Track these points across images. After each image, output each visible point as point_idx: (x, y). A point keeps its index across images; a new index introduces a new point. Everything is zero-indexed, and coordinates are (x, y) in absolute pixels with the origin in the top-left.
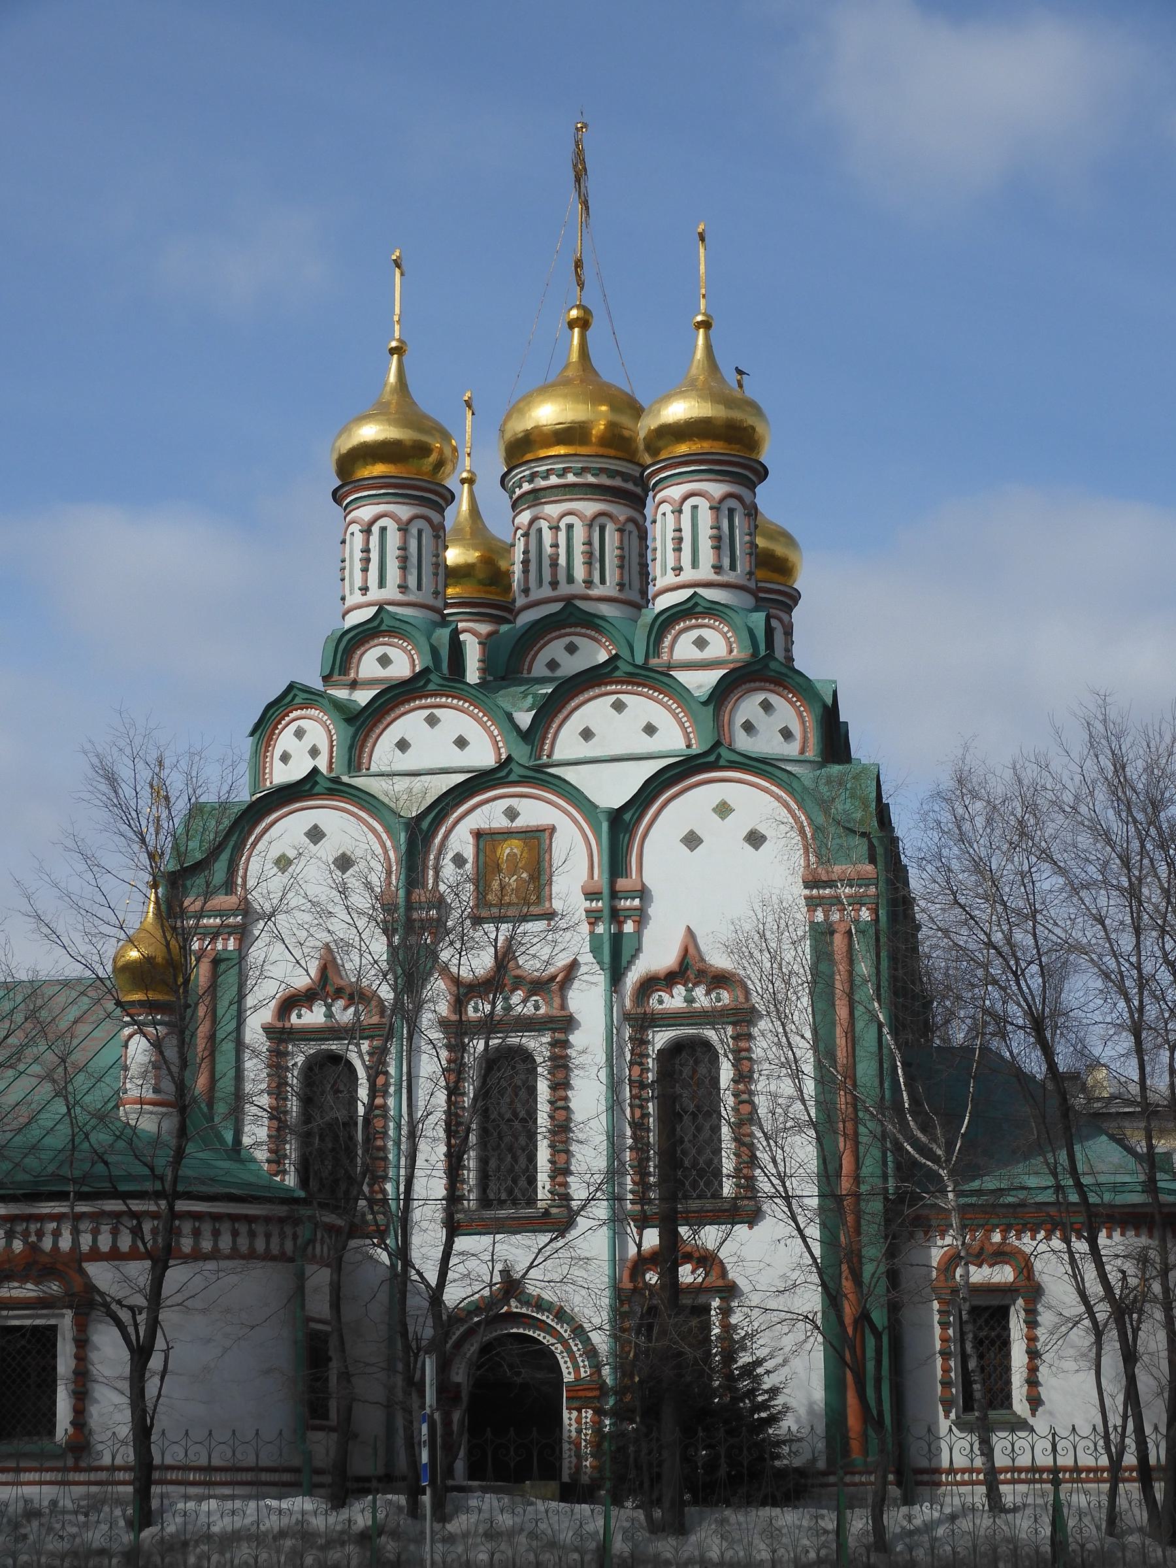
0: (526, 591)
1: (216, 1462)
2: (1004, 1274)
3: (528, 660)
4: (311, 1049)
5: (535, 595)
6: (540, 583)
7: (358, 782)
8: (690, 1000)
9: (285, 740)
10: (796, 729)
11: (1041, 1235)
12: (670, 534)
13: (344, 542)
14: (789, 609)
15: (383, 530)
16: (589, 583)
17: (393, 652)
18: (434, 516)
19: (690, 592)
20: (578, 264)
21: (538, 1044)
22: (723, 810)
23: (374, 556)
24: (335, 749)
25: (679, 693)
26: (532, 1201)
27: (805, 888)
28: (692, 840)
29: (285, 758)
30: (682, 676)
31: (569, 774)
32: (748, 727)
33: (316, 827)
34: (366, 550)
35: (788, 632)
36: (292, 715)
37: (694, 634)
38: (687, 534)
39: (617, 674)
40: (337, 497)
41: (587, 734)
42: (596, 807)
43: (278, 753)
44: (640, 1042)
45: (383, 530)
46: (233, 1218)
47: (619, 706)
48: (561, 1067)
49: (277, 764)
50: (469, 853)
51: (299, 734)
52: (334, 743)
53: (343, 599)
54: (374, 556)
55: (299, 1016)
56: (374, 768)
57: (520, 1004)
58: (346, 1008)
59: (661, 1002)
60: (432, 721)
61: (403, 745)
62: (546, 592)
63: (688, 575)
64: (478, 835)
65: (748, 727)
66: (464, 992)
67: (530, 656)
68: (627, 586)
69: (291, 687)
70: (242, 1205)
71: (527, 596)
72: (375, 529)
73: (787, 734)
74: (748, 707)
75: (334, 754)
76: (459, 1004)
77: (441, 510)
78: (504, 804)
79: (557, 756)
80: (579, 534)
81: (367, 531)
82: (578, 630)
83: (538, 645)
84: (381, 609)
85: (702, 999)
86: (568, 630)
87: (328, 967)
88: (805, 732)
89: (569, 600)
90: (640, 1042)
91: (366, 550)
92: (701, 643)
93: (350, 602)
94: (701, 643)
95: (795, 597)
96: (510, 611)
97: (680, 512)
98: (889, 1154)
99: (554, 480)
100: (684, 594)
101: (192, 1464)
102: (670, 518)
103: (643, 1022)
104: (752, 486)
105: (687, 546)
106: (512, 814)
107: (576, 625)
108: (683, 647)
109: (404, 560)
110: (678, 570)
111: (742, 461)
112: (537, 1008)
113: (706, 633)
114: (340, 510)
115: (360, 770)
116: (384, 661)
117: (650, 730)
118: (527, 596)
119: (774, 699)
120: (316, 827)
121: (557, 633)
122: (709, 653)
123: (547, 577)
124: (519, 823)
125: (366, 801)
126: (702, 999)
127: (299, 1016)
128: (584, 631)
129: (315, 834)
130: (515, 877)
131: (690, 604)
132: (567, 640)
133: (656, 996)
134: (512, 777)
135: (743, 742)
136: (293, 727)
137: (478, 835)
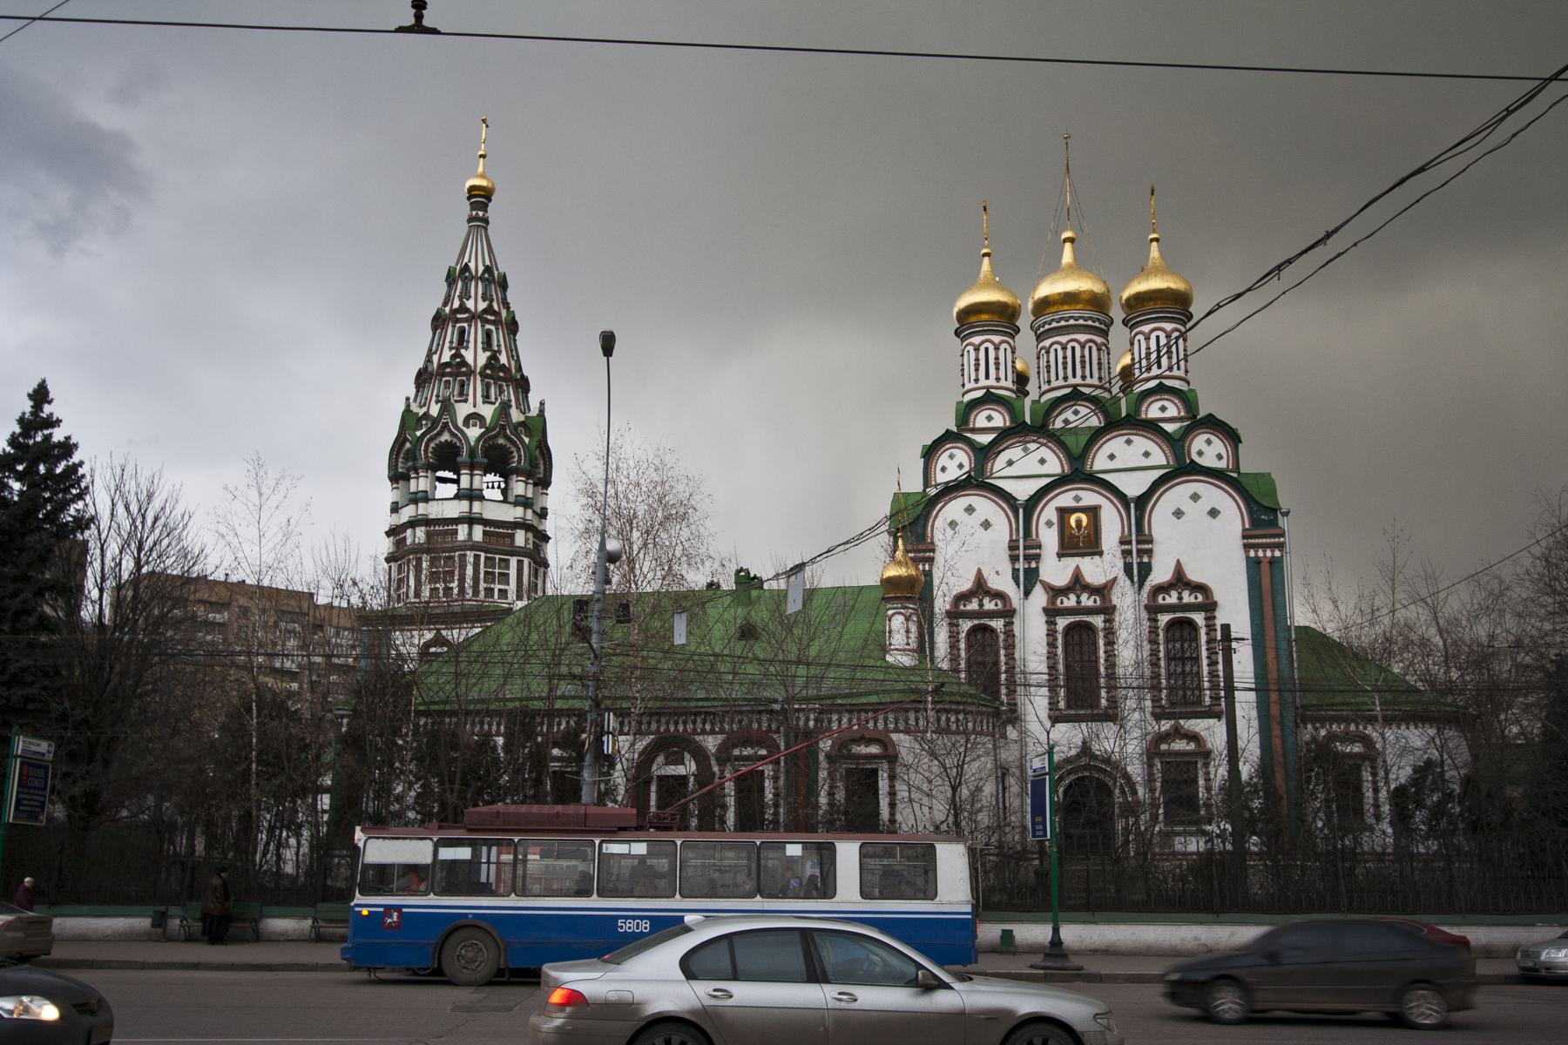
2: (1357, 748)
4: (1072, 619)
5: (1054, 384)
6: (1057, 379)
8: (1180, 598)
9: (943, 460)
10: (1224, 454)
11: (1403, 727)
12: (973, 362)
13: (962, 355)
15: (987, 349)
16: (1170, 368)
17: (994, 414)
21: (1098, 621)
23: (982, 363)
26: (1098, 705)
29: (943, 469)
34: (977, 359)
37: (1159, 404)
40: (957, 333)
41: (1112, 457)
44: (1153, 620)
47: (1129, 442)
48: (1110, 633)
53: (963, 385)
54: (982, 363)
55: (965, 606)
57: (1087, 601)
58: (1088, 598)
59: (1062, 603)
61: (1112, 457)
62: (1061, 382)
66: (1055, 592)
69: (947, 431)
73: (1220, 457)
76: (1052, 600)
78: (1074, 493)
80: (1163, 341)
81: (977, 349)
85: (1187, 598)
87: (980, 581)
88: (1228, 456)
89: (1075, 387)
90: (1153, 620)
91: (977, 359)
92: (989, 418)
93: (968, 386)
94: (989, 418)
97: (1149, 338)
102: (1143, 342)
103: (1153, 610)
104: (1013, 337)
106: (1077, 499)
108: (980, 420)
109: (997, 364)
110: (977, 380)
113: (1166, 403)
114: (959, 340)
117: (1147, 454)
119: (1213, 438)
123: (973, 377)
124: (1082, 504)
126: (1187, 598)
127: (965, 606)
129: (970, 510)
136: (948, 452)
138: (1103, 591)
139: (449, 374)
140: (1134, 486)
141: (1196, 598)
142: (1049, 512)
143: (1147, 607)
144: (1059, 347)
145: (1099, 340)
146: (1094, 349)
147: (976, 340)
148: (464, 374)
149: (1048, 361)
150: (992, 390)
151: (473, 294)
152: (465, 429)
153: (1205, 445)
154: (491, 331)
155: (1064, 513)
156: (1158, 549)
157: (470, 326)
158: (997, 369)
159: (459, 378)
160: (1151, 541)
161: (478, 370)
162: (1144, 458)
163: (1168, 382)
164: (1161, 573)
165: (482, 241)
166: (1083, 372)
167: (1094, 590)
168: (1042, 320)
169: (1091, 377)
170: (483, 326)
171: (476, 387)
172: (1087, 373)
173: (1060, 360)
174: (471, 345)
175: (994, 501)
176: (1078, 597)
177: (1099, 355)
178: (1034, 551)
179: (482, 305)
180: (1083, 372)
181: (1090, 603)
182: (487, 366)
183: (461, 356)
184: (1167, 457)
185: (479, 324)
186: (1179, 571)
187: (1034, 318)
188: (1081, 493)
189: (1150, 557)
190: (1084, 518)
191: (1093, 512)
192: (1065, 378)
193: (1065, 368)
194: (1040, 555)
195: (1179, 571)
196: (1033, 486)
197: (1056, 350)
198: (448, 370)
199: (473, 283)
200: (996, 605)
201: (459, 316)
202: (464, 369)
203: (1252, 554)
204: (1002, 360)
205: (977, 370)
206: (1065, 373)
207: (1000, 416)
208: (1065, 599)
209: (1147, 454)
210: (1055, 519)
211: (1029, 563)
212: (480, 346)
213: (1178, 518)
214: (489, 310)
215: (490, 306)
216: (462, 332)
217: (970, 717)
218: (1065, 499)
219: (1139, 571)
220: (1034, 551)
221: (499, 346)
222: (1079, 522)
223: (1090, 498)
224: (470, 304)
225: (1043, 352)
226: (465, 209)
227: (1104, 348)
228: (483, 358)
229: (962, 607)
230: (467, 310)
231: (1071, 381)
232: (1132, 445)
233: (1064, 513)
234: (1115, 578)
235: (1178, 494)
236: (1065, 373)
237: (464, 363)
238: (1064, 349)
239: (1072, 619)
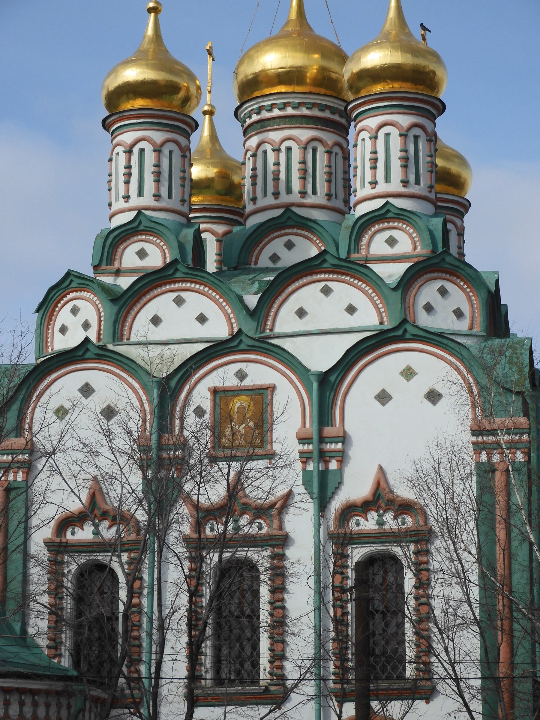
0: (254, 200)
3: (255, 254)
4: (83, 559)
5: (261, 203)
7: (121, 349)
8: (381, 523)
10: (466, 310)
12: (368, 156)
14: (462, 216)
15: (142, 151)
16: (303, 194)
23: (135, 171)
24: (102, 323)
27: (473, 435)
29: (63, 330)
30: (377, 268)
31: (287, 344)
32: (429, 308)
33: (87, 384)
34: (128, 167)
35: (461, 234)
36: (69, 296)
37: (386, 234)
38: (381, 155)
39: (326, 265)
41: (301, 313)
43: (57, 326)
46: (21, 691)
47: (326, 291)
49: (57, 334)
50: (207, 406)
51: (75, 311)
52: (102, 319)
53: (110, 205)
54: (135, 171)
55: (73, 533)
56: (133, 339)
58: (110, 527)
59: (358, 524)
60: (179, 302)
62: (270, 200)
63: (382, 188)
64: (215, 392)
65: (429, 308)
67: (257, 251)
68: (334, 196)
69: (69, 274)
71: (255, 204)
72: (136, 150)
73: (459, 314)
75: (102, 328)
76: (198, 526)
77: (187, 136)
78: (235, 367)
79: (278, 330)
82: (295, 230)
83: (263, 243)
84: (139, 213)
86: (287, 231)
89: (287, 207)
91: (128, 167)
95: (466, 206)
96: (241, 215)
97: (376, 138)
99: (276, 112)
102: (368, 143)
104: (433, 118)
105: (381, 165)
107: (293, 227)
109: (158, 175)
110: (127, 198)
111: (425, 98)
112: (260, 528)
113: (395, 234)
114: (108, 135)
115: (122, 340)
116: (142, 254)
118: (255, 204)
119: (449, 286)
120: (87, 384)
122: (398, 250)
124: (247, 382)
127: (73, 533)
128: (299, 231)
130: (244, 425)
131: (383, 211)
132: (286, 239)
133: (354, 520)
134: (242, 347)
136: (70, 306)
137: (215, 392)
141: (404, 523)
143: (331, 536)
145: (330, 138)
146: (321, 150)
147: (128, 137)
150: (294, 209)
158: (158, 181)
169: (314, 192)
172: (164, 191)
175: (121, 378)
176: (96, 526)
184: (380, 314)
187: (107, 113)
188: (250, 369)
192: (276, 194)
203: (484, 458)
205: (127, 182)
206: (276, 187)
207: (158, 252)
208: (362, 520)
209: (351, 310)
211: (327, 462)
213: (383, 404)
217: (41, 700)
225: (249, 153)
227: (337, 149)
229: (69, 536)
231: (284, 198)
234: (289, 495)
236: (276, 187)
239: (83, 559)
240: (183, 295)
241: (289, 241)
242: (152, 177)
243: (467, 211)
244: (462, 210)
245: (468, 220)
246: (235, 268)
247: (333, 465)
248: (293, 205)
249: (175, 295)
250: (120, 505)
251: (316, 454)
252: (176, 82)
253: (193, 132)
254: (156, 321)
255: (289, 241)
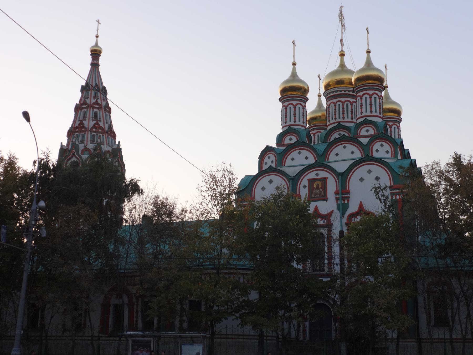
0: (329, 121)
1: (240, 333)
5: (331, 122)
7: (281, 169)
9: (266, 160)
12: (360, 104)
14: (399, 123)
18: (303, 104)
19: (364, 119)
20: (26, 115)
22: (369, 172)
23: (337, 111)
25: (360, 144)
27: (390, 190)
28: (362, 180)
29: (266, 163)
30: (361, 140)
31: (332, 165)
32: (377, 151)
33: (271, 180)
35: (399, 128)
36: (267, 153)
41: (337, 154)
42: (337, 172)
45: (332, 106)
47: (345, 147)
49: (264, 165)
51: (269, 158)
54: (337, 111)
56: (286, 165)
59: (354, 220)
60: (300, 153)
62: (334, 121)
63: (364, 114)
64: (309, 180)
70: (247, 271)
73: (387, 152)
74: (377, 146)
77: (305, 103)
79: (330, 160)
82: (342, 130)
89: (339, 123)
92: (367, 131)
94: (367, 131)
95: (401, 120)
96: (326, 126)
98: (326, 251)
100: (363, 119)
101: (234, 334)
106: (317, 175)
110: (362, 113)
111: (377, 85)
113: (369, 128)
115: (282, 166)
117: (353, 153)
119: (384, 143)
120: (271, 180)
121: (336, 131)
123: (334, 117)
124: (319, 177)
125: (283, 174)
128: (343, 130)
129: (271, 182)
132: (339, 132)
134: (317, 166)
135: (375, 155)
136: (268, 156)
137: (309, 180)
138: (328, 217)
139: (77, 132)
140: (341, 167)
142: (305, 182)
144: (292, 107)
146: (349, 104)
148: (83, 131)
149: (361, 103)
151: (89, 97)
152: (82, 156)
153: (380, 147)
154: (97, 112)
155: (311, 181)
156: (352, 196)
157: (87, 110)
159: (81, 133)
160: (348, 192)
161: (89, 129)
162: (305, 160)
163: (369, 118)
164: (353, 208)
165: (93, 73)
166: (343, 115)
167: (323, 217)
168: (328, 92)
169: (299, 121)
170: (93, 110)
171: (88, 136)
173: (292, 113)
174: (87, 119)
177: (352, 107)
178: (346, 196)
179: (93, 101)
180: (343, 115)
181: (322, 223)
182: (94, 127)
183: (98, 124)
185: (91, 109)
186: (361, 206)
189: (348, 200)
190: (320, 183)
191: (324, 180)
192: (335, 119)
193: (343, 114)
194: (349, 197)
195: (361, 206)
196: (346, 165)
197: (290, 108)
198: (77, 130)
199: (90, 92)
200: (324, 222)
201: (83, 106)
202: (83, 129)
204: (373, 103)
208: (356, 219)
209: (353, 153)
210: (307, 185)
211: (344, 201)
212: (91, 119)
214: (96, 103)
215: (97, 101)
216: (85, 114)
218: (312, 175)
219: (343, 208)
220: (346, 196)
221: (100, 118)
222: (318, 186)
223: (323, 174)
224: (88, 101)
226: (89, 59)
228: (92, 123)
230: (98, 104)
232: (346, 148)
233: (311, 181)
235: (361, 171)
237: (83, 127)
238: (335, 105)
240: (301, 151)
241: (340, 133)
242: (293, 116)
243: (401, 121)
244: (306, 101)
245: (402, 124)
246: (323, 143)
247: (346, 202)
248: (341, 122)
249: (298, 151)
250: (133, 223)
251: (340, 198)
252: (392, 108)
253: (307, 101)
254: (293, 159)
255: (340, 133)
